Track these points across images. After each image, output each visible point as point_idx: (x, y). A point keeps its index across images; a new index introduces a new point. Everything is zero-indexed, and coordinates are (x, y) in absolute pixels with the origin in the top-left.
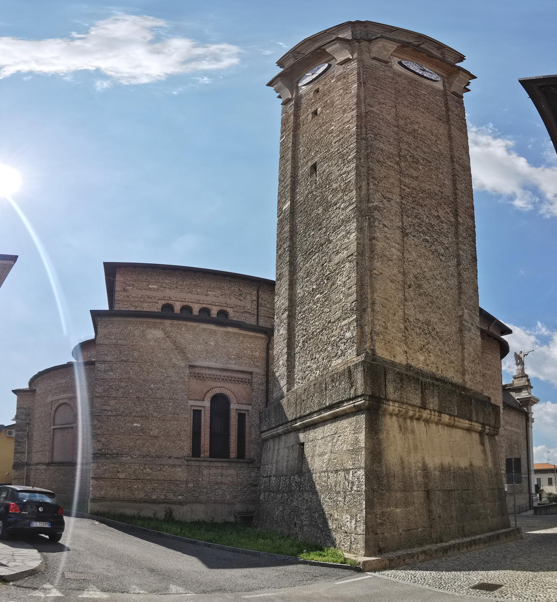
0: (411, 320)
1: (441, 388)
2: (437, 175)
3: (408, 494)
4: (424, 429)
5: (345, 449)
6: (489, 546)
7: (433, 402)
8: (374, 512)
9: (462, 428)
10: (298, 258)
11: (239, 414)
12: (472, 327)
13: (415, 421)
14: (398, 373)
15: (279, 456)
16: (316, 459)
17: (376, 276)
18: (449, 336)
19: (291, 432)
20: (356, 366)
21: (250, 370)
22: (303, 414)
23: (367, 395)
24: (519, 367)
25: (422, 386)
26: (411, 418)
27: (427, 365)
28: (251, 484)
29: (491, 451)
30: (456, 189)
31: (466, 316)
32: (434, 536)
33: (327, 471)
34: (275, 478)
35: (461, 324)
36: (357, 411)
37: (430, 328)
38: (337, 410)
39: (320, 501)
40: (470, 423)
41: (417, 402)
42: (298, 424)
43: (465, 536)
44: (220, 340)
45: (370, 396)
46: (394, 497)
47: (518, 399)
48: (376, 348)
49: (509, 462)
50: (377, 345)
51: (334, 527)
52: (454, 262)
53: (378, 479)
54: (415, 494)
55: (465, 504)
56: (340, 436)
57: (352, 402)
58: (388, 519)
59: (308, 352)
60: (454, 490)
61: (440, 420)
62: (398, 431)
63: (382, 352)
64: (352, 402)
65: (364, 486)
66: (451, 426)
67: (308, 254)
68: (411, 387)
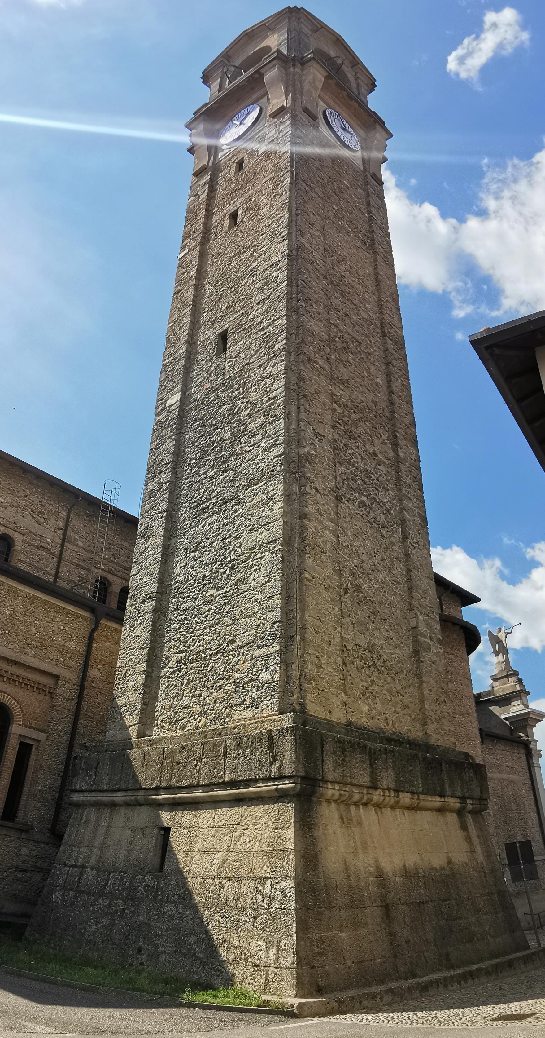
0: (349, 648)
1: (397, 754)
2: (368, 370)
3: (357, 911)
4: (375, 817)
5: (256, 848)
6: (495, 979)
7: (387, 778)
8: (308, 938)
9: (431, 810)
10: (183, 510)
11: (21, 743)
12: (432, 643)
13: (361, 807)
14: (339, 741)
15: (105, 839)
16: (197, 857)
17: (307, 583)
18: (400, 665)
19: (141, 805)
20: (282, 732)
21: (56, 671)
22: (173, 782)
23: (298, 777)
24: (501, 658)
25: (370, 756)
26: (356, 804)
27: (373, 718)
28: (17, 867)
29: (478, 836)
30: (392, 392)
31: (422, 628)
32: (401, 969)
33: (219, 876)
34: (94, 872)
35: (416, 641)
36: (280, 797)
37: (374, 656)
38: (245, 790)
39: (201, 919)
40: (442, 800)
41: (365, 779)
42: (160, 797)
43: (452, 967)
44: (20, 609)
45: (303, 778)
46: (337, 917)
47: (505, 719)
48: (307, 701)
49: (510, 848)
50: (309, 696)
51: (232, 957)
52: (398, 535)
53: (314, 893)
54: (368, 911)
55: (447, 920)
56: (247, 829)
57: (272, 783)
58: (330, 946)
59: (185, 682)
60: (427, 902)
61: (397, 802)
62: (339, 824)
63: (314, 709)
64: (272, 783)
65: (293, 903)
66: (413, 809)
67: (201, 510)
68: (356, 759)
